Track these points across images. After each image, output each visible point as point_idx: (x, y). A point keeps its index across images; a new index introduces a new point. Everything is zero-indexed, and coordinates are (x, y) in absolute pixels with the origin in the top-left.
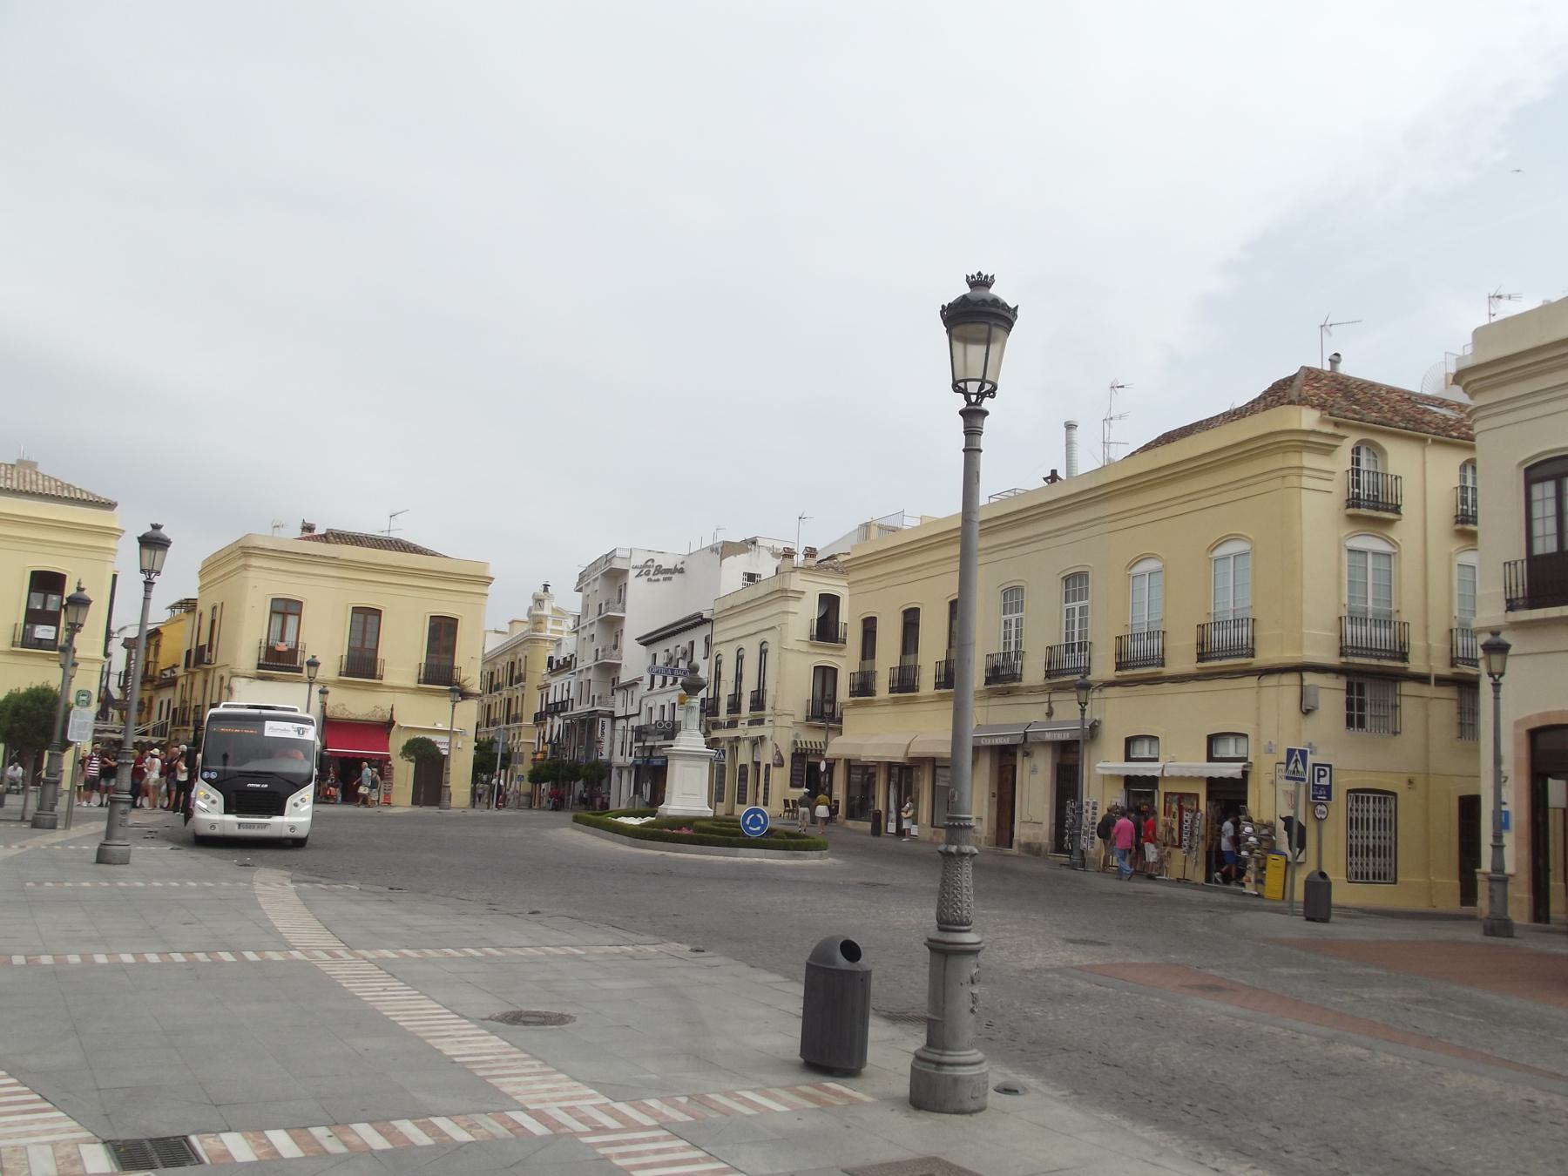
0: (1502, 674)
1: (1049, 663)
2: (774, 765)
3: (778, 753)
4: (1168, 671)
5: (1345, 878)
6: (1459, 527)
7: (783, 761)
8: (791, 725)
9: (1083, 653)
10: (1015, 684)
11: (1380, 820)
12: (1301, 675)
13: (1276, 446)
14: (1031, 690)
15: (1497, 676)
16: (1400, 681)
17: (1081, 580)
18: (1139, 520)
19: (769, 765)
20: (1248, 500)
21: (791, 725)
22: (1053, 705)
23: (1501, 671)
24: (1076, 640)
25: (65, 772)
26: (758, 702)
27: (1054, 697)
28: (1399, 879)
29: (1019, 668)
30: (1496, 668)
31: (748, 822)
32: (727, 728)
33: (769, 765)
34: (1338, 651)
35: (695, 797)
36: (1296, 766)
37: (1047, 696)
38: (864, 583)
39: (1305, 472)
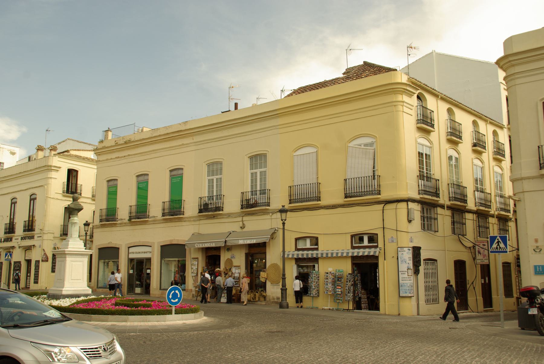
0: (285, 220)
1: (290, 196)
2: (42, 261)
3: (45, 254)
4: (322, 203)
5: (425, 303)
6: (449, 137)
7: (48, 258)
8: (52, 239)
9: (254, 197)
10: (221, 212)
11: (433, 273)
12: (408, 203)
13: (392, 90)
14: (229, 215)
15: (284, 221)
16: (437, 207)
17: (261, 160)
18: (373, 113)
19: (39, 261)
20: (359, 119)
21: (52, 239)
22: (244, 222)
23: (285, 219)
24: (215, 194)
25: (411, 207)
26: (30, 227)
27: (245, 218)
28: (440, 301)
29: (182, 208)
30: (284, 218)
31: (171, 297)
32: (4, 242)
33: (39, 261)
34: (417, 192)
35: (79, 281)
36: (498, 245)
37: (241, 218)
38: (125, 158)
39: (405, 104)
